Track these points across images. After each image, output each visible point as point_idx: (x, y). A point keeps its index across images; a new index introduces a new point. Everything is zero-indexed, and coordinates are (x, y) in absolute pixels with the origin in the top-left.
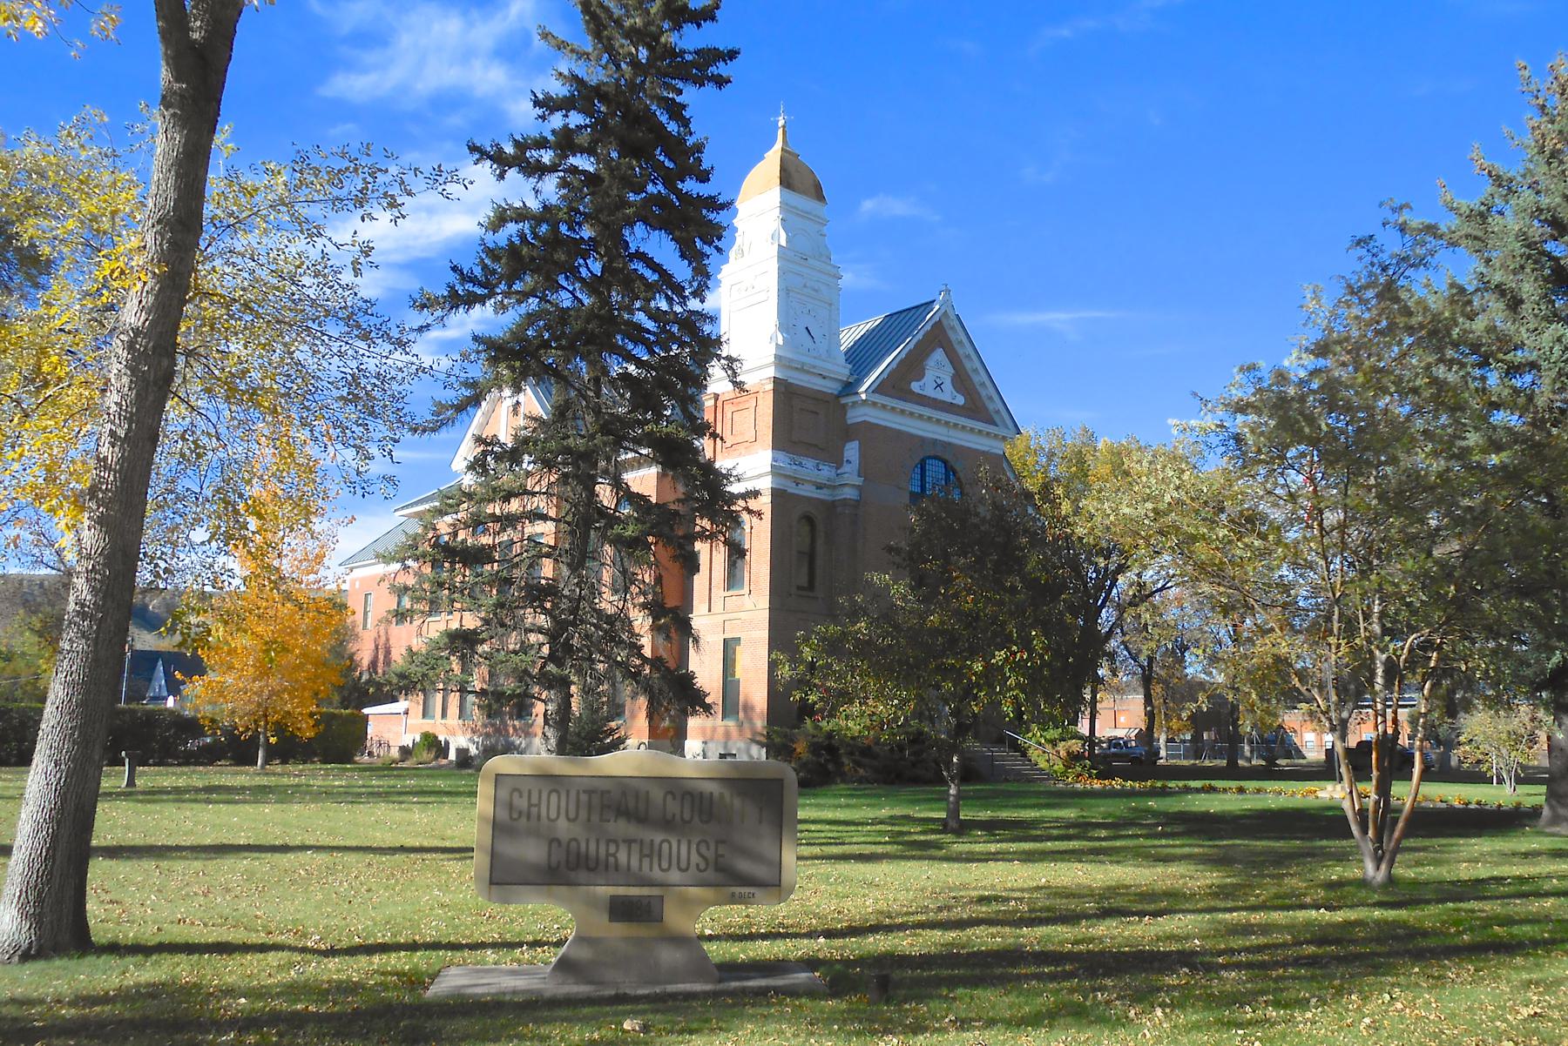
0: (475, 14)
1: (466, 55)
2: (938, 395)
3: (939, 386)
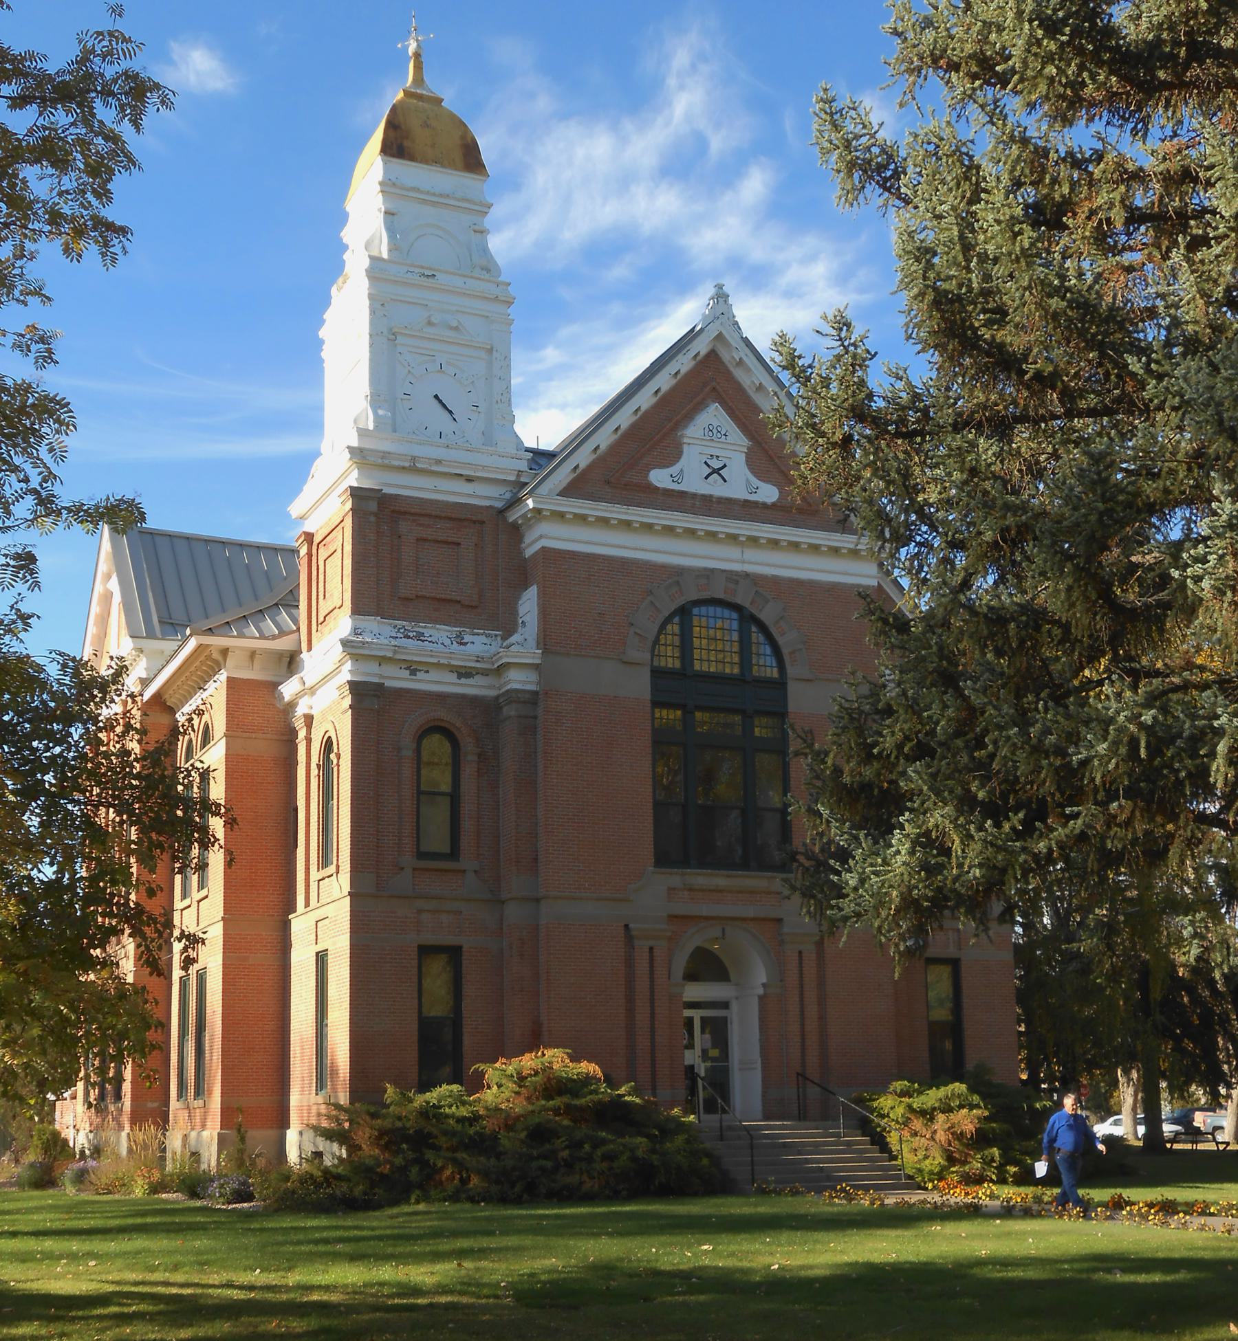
0: (628, 126)
1: (624, 182)
2: (715, 488)
3: (716, 471)
